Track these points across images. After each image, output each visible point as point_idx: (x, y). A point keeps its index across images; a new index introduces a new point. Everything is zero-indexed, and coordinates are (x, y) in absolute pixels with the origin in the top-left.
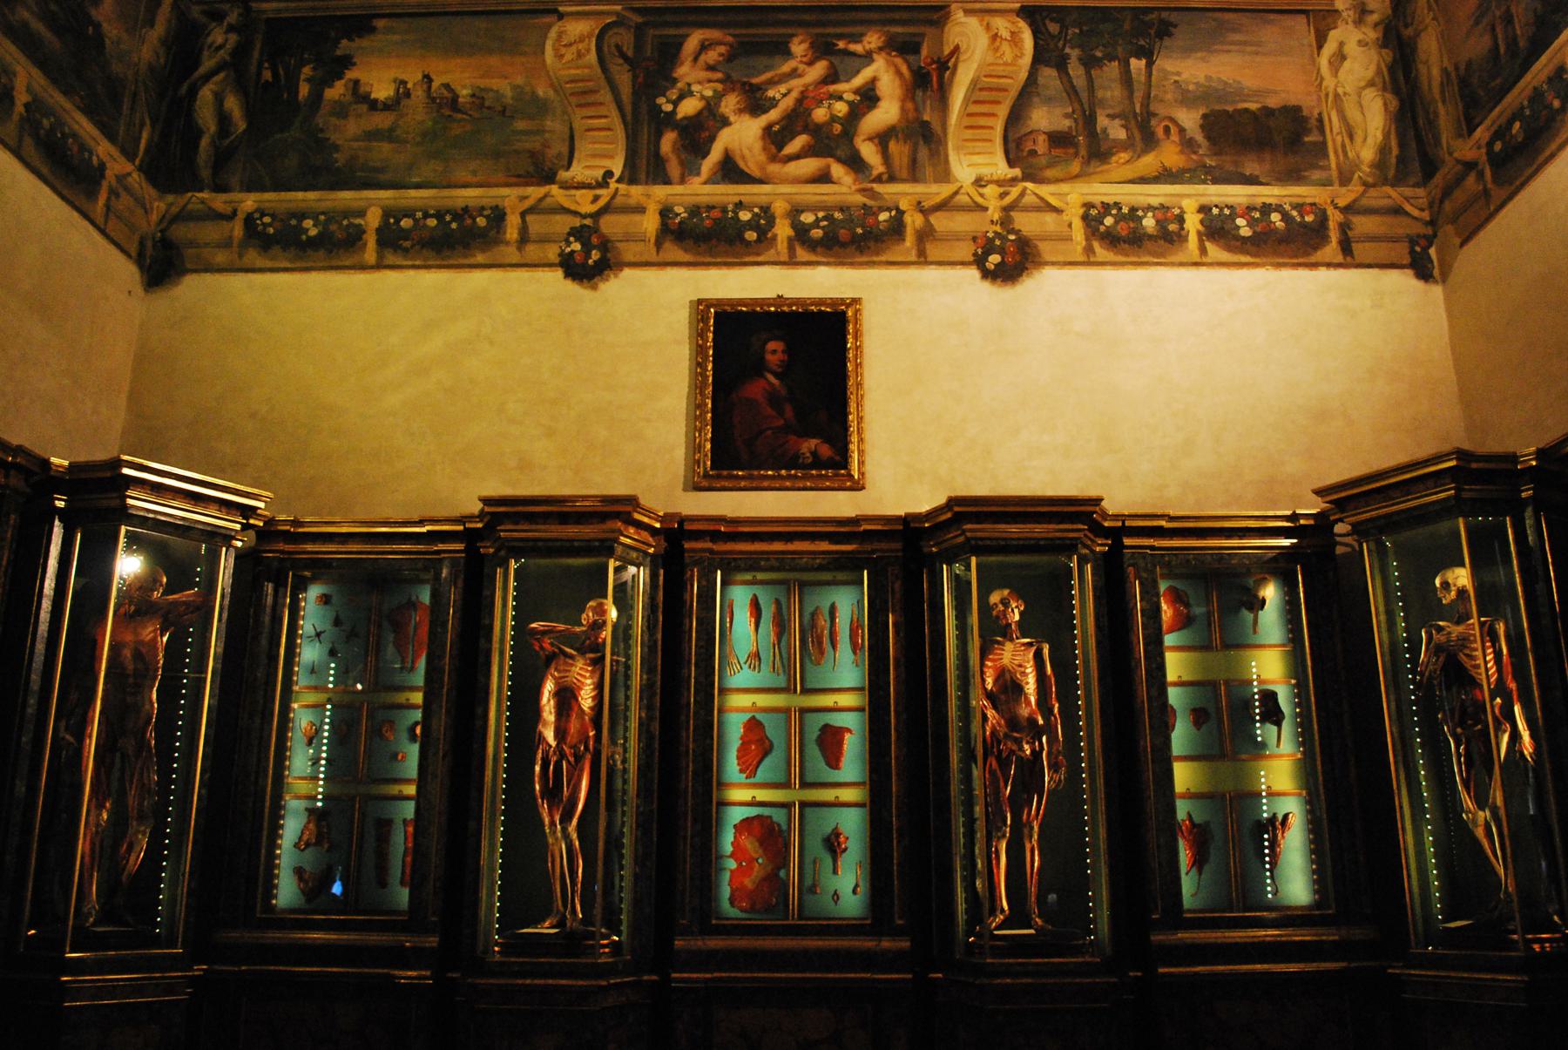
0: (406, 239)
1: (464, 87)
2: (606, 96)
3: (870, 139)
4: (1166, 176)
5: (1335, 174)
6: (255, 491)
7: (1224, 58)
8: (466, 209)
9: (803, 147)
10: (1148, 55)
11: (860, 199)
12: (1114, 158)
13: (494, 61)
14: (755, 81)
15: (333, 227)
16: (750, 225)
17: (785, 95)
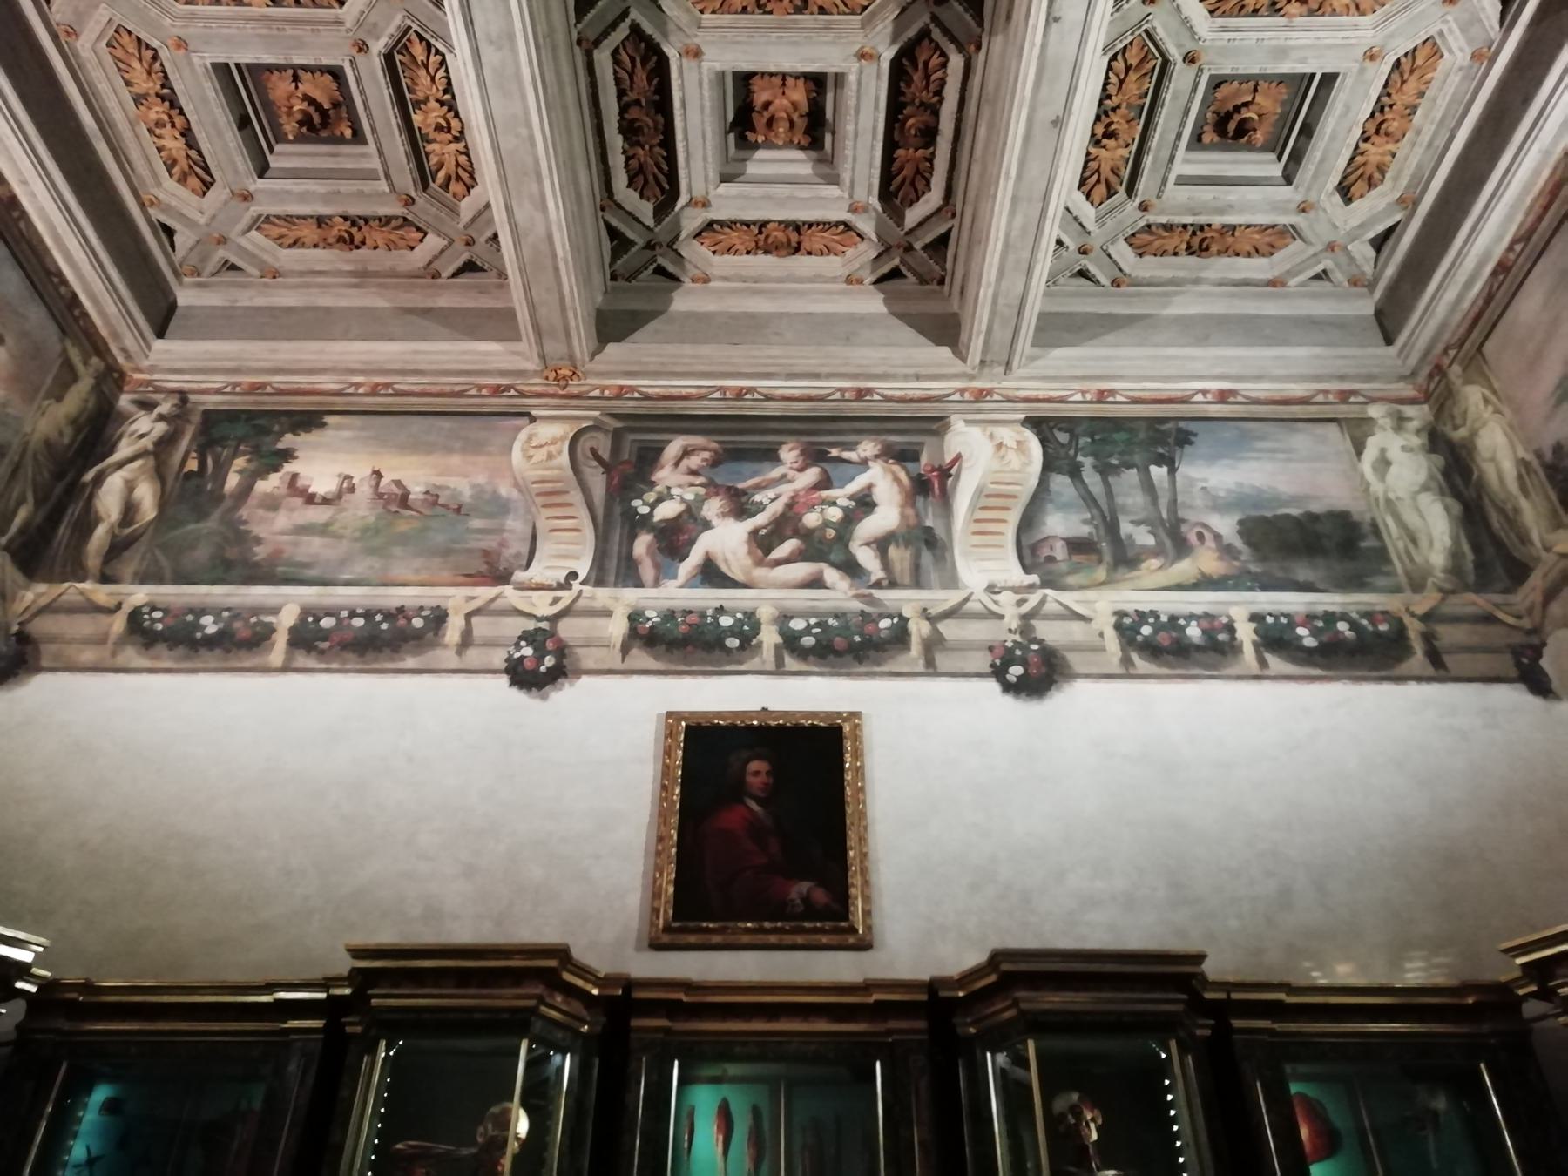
0: (325, 639)
1: (418, 484)
2: (576, 497)
3: (868, 544)
4: (1205, 583)
5: (1403, 580)
6: (21, 935)
7: (1254, 465)
8: (401, 610)
9: (792, 553)
10: (1170, 463)
11: (857, 605)
12: (1144, 565)
13: (455, 460)
14: (740, 486)
15: (237, 625)
16: (731, 632)
17: (773, 500)
